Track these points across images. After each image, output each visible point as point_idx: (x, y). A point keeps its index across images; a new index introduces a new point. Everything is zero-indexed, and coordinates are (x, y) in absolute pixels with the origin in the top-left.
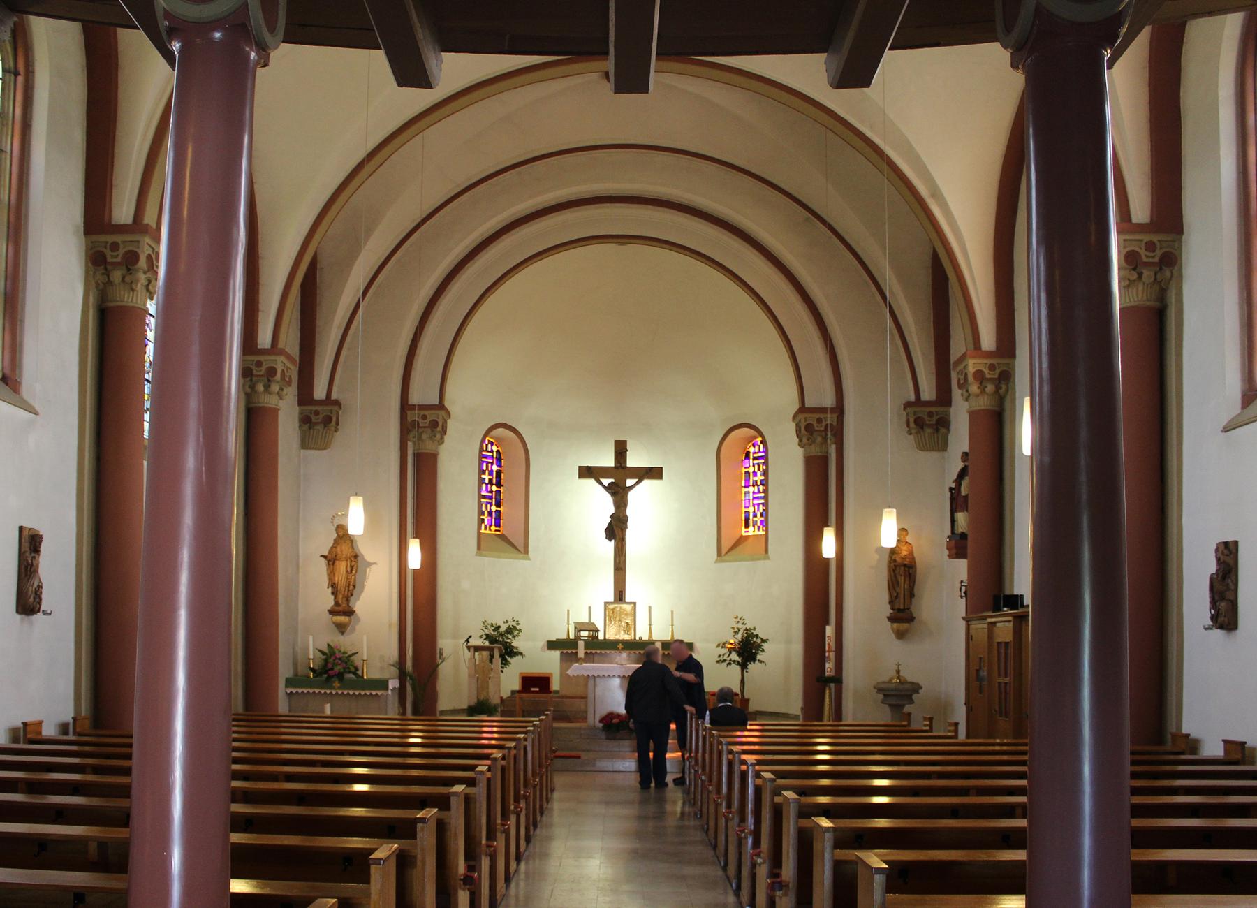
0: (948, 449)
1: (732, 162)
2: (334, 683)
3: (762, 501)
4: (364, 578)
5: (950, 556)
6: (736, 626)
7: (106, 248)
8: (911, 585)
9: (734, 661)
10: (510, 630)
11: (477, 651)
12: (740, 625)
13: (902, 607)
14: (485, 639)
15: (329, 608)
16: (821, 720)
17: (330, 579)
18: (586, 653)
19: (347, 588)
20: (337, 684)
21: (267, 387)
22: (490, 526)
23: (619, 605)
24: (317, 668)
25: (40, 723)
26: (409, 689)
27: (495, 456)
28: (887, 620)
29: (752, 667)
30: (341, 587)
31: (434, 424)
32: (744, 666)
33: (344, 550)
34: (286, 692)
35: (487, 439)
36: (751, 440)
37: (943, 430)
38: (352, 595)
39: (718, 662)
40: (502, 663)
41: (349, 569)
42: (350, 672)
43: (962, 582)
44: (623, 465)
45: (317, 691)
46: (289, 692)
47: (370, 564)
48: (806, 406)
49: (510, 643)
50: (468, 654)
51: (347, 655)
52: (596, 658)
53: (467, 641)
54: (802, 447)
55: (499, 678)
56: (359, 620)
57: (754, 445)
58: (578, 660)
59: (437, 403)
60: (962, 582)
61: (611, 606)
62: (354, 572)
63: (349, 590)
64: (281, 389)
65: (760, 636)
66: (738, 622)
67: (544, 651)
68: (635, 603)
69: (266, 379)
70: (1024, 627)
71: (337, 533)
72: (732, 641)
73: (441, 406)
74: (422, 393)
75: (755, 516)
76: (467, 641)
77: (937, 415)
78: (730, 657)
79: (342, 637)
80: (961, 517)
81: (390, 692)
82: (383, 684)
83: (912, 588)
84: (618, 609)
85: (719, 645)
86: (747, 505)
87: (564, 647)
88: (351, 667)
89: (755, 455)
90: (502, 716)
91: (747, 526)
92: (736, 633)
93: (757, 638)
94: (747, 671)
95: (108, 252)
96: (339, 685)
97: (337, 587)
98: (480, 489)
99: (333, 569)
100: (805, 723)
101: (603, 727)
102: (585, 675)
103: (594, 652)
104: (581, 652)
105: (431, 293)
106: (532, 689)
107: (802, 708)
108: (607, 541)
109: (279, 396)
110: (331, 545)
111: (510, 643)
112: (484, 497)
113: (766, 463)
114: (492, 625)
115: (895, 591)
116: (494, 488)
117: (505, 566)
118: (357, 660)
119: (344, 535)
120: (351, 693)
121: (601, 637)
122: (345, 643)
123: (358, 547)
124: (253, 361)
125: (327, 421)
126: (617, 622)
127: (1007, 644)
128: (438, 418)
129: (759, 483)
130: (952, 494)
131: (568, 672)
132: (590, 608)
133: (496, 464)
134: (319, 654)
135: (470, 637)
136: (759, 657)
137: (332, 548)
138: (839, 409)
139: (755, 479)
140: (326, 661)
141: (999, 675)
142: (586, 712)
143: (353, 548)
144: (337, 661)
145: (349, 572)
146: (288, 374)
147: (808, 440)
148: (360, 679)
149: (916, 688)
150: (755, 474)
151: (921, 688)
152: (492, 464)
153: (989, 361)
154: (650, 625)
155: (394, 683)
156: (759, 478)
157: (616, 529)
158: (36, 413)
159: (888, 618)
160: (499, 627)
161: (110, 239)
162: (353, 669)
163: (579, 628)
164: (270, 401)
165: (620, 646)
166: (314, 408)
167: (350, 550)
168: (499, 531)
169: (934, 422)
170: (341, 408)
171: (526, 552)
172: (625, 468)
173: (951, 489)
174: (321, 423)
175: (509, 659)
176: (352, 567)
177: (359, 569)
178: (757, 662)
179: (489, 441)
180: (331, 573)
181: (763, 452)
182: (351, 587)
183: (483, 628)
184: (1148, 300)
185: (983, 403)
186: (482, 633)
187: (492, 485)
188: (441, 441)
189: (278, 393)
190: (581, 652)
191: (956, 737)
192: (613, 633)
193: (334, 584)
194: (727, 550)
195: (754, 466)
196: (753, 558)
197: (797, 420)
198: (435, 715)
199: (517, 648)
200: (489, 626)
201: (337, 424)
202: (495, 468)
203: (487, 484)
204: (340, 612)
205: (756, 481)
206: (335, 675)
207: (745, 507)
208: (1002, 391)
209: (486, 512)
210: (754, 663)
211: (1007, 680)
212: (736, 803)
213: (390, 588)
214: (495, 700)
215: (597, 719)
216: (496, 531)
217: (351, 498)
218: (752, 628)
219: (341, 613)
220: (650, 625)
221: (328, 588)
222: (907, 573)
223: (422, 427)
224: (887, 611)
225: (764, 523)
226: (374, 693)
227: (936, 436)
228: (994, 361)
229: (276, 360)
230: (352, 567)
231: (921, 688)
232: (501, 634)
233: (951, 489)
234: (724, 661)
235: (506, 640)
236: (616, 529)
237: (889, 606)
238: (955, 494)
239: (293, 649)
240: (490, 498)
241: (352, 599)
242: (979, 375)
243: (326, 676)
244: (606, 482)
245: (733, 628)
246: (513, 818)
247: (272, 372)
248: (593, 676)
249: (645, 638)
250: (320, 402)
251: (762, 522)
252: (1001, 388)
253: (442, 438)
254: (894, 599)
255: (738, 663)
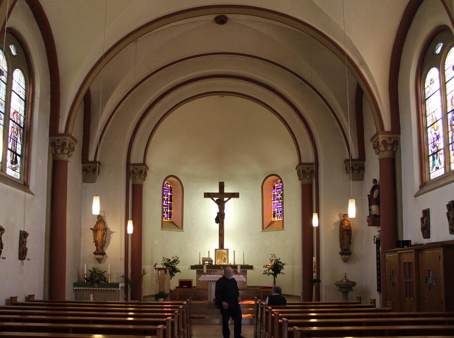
0: (364, 180)
1: (269, 59)
2: (95, 285)
3: (281, 206)
4: (110, 239)
5: (369, 225)
6: (271, 258)
7: (56, 141)
8: (350, 238)
9: (271, 273)
10: (175, 261)
11: (159, 270)
12: (273, 258)
13: (346, 248)
14: (164, 265)
15: (94, 252)
16: (311, 301)
17: (94, 239)
18: (207, 271)
19: (102, 243)
20: (96, 285)
21: (62, 151)
22: (167, 218)
23: (221, 250)
24: (88, 278)
25: (16, 297)
26: (129, 287)
27: (169, 189)
28: (339, 254)
29: (278, 275)
30: (99, 242)
31: (141, 172)
32: (275, 275)
33: (101, 226)
34: (74, 289)
35: (166, 182)
36: (276, 181)
37: (362, 172)
38: (104, 246)
39: (264, 274)
40: (170, 275)
41: (103, 235)
42: (102, 280)
43: (375, 236)
44: (223, 192)
45: (87, 289)
46: (75, 289)
47: (112, 232)
48: (302, 162)
49: (175, 267)
50: (155, 272)
51: (101, 272)
52: (211, 272)
53: (155, 266)
54: (300, 181)
55: (169, 282)
56: (107, 257)
57: (277, 183)
58: (204, 274)
59: (143, 163)
60: (375, 236)
61: (218, 251)
62: (105, 236)
63: (103, 244)
64: (69, 152)
65: (282, 262)
66: (273, 256)
67: (190, 270)
68: (228, 249)
69: (62, 147)
70: (420, 255)
71: (98, 219)
72: (270, 265)
73: (144, 164)
74: (136, 158)
75: (278, 212)
76: (155, 266)
77: (359, 165)
78: (269, 271)
79: (100, 264)
80: (374, 207)
81: (120, 289)
82: (117, 285)
83: (350, 240)
84: (221, 252)
85: (264, 266)
86: (274, 208)
87: (198, 268)
88: (103, 278)
89: (277, 188)
90: (171, 300)
91: (274, 217)
92: (271, 261)
93: (280, 263)
94: (276, 278)
95: (56, 142)
96: (97, 286)
97: (98, 243)
98: (163, 203)
99: (96, 234)
100: (304, 302)
101: (215, 303)
102: (207, 280)
103: (211, 270)
104: (205, 270)
105: (140, 116)
106: (184, 286)
107: (302, 293)
108: (216, 224)
109: (68, 155)
110: (95, 224)
111: (175, 267)
112: (165, 206)
113: (282, 190)
114: (167, 259)
115: (343, 241)
116: (169, 202)
117: (174, 235)
118: (106, 275)
119: (101, 220)
120: (103, 289)
121: (214, 264)
122: (101, 267)
123: (107, 225)
124: (56, 139)
125: (94, 170)
126: (220, 257)
127: (410, 263)
128: (143, 169)
129: (279, 199)
130: (369, 198)
131: (199, 279)
132: (209, 252)
133: (170, 192)
134: (89, 272)
135: (156, 264)
136: (281, 271)
137: (95, 225)
138: (317, 163)
139: (278, 197)
140: (92, 275)
141: (405, 278)
142: (207, 296)
143: (105, 225)
144: (97, 275)
145: (103, 236)
146: (72, 146)
147: (303, 177)
148: (106, 283)
149: (354, 284)
150: (277, 195)
151: (356, 284)
152: (168, 192)
153: (388, 136)
154: (234, 258)
155: (121, 285)
156: (279, 197)
157: (220, 218)
158: (33, 194)
159: (339, 253)
160: (170, 260)
161: (57, 138)
162: (104, 279)
163: (204, 260)
164: (64, 157)
165: (222, 267)
166: (88, 165)
167: (103, 226)
168: (171, 220)
169: (358, 168)
170: (101, 165)
171: (182, 229)
172: (223, 193)
173: (369, 195)
174: (91, 171)
175: (174, 273)
176: (104, 234)
177: (107, 234)
178: (281, 274)
179: (167, 183)
180: (95, 236)
181: (281, 186)
182: (104, 243)
183: (163, 260)
184: (389, 156)
185: (386, 155)
186: (163, 262)
187: (168, 201)
188: (144, 180)
189: (67, 154)
190: (205, 270)
191: (374, 306)
192: (219, 262)
193: (96, 241)
194: (266, 227)
195: (277, 192)
196: (278, 230)
197: (298, 169)
198: (140, 300)
199: (177, 269)
200: (166, 260)
201: (99, 172)
202: (169, 194)
203: (165, 201)
204: (98, 253)
205: (278, 198)
206: (95, 281)
207: (273, 209)
208: (394, 149)
209: (165, 212)
210: (280, 274)
211: (411, 280)
212: (270, 330)
213: (121, 242)
214: (167, 292)
215: (212, 300)
216: (169, 220)
217: (94, 197)
218: (278, 259)
219: (99, 254)
220: (234, 258)
221: (94, 243)
222: (348, 234)
223: (135, 173)
224: (339, 250)
225: (282, 215)
226: (113, 289)
227: (359, 174)
228: (391, 136)
229: (66, 139)
230: (104, 234)
231: (356, 284)
232: (171, 263)
233: (369, 195)
234: (267, 273)
235: (173, 265)
236: (220, 218)
237: (340, 248)
238: (370, 197)
239: (78, 270)
240: (167, 206)
241: (104, 248)
242: (384, 142)
243: (92, 282)
244: (215, 199)
245: (270, 259)
246: (186, 329)
247: (64, 144)
248: (210, 280)
249: (232, 264)
250: (91, 162)
251: (281, 215)
252: (394, 148)
253: (144, 178)
254: (342, 245)
255: (273, 274)
